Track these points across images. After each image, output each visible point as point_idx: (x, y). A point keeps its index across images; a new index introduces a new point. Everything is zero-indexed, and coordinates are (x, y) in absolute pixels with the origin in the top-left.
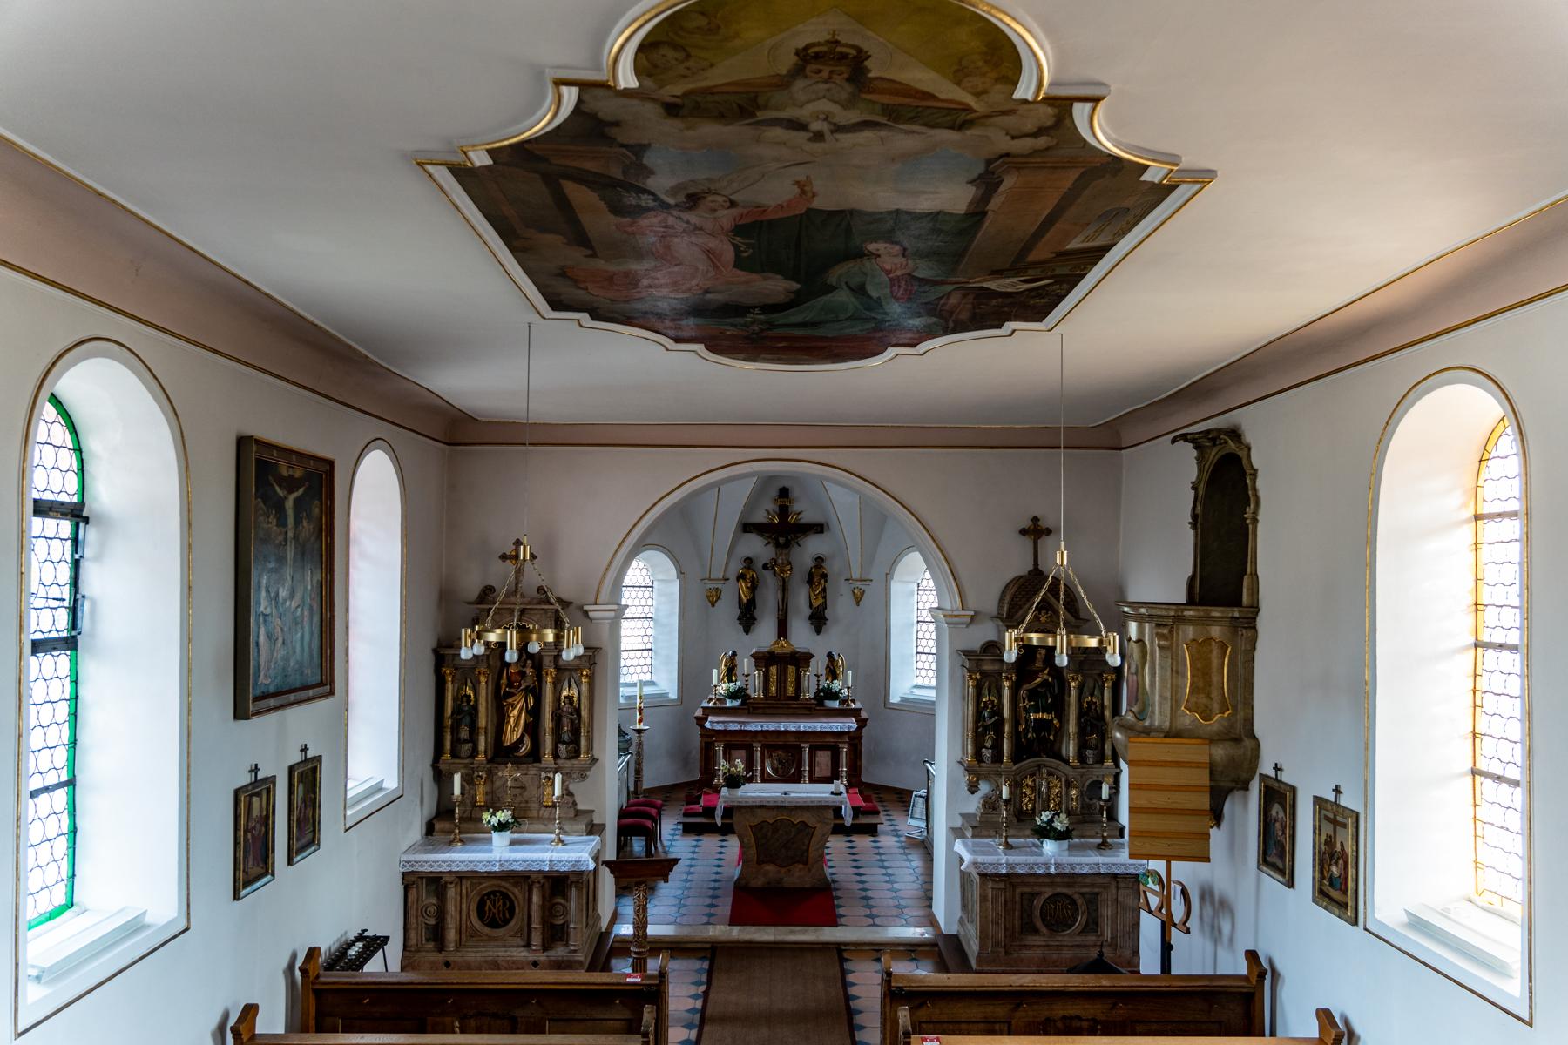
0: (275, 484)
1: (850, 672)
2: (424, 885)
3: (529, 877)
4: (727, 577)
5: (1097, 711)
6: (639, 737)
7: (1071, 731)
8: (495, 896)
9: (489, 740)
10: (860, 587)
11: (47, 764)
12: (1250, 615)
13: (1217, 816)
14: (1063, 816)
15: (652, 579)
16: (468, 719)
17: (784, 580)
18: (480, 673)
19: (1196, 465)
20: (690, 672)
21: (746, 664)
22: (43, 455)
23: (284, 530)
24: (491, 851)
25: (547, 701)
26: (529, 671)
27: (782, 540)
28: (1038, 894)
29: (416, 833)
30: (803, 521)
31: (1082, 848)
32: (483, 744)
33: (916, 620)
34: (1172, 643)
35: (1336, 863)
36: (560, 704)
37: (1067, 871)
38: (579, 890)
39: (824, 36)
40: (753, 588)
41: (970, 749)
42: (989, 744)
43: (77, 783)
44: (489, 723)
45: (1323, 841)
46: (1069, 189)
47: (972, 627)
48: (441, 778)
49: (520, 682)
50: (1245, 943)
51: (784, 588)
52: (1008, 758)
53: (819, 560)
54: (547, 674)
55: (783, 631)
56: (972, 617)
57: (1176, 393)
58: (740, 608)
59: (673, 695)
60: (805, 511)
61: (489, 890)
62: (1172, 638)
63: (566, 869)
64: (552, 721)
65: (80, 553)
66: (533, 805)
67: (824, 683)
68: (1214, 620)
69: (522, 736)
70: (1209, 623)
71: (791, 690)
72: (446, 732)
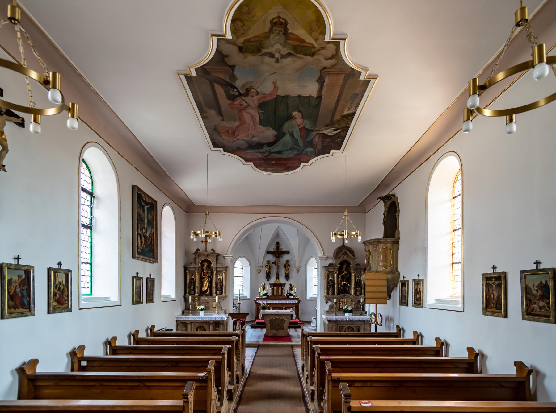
1: (296, 289)
3: (209, 322)
4: (263, 266)
6: (239, 305)
11: (85, 257)
13: (389, 297)
14: (350, 307)
16: (193, 284)
17: (278, 266)
20: (253, 291)
21: (268, 287)
22: (83, 176)
23: (144, 214)
24: (199, 315)
26: (209, 272)
27: (277, 255)
28: (344, 327)
29: (180, 312)
33: (313, 285)
34: (377, 249)
35: (418, 294)
37: (351, 320)
38: (223, 326)
39: (276, 15)
40: (270, 268)
41: (326, 292)
42: (331, 290)
43: (92, 264)
46: (342, 84)
47: (327, 261)
48: (186, 300)
51: (278, 268)
53: (288, 261)
54: (214, 272)
55: (278, 278)
57: (379, 184)
59: (248, 297)
60: (283, 248)
61: (199, 326)
63: (219, 320)
65: (92, 205)
67: (289, 292)
69: (207, 289)
71: (280, 293)
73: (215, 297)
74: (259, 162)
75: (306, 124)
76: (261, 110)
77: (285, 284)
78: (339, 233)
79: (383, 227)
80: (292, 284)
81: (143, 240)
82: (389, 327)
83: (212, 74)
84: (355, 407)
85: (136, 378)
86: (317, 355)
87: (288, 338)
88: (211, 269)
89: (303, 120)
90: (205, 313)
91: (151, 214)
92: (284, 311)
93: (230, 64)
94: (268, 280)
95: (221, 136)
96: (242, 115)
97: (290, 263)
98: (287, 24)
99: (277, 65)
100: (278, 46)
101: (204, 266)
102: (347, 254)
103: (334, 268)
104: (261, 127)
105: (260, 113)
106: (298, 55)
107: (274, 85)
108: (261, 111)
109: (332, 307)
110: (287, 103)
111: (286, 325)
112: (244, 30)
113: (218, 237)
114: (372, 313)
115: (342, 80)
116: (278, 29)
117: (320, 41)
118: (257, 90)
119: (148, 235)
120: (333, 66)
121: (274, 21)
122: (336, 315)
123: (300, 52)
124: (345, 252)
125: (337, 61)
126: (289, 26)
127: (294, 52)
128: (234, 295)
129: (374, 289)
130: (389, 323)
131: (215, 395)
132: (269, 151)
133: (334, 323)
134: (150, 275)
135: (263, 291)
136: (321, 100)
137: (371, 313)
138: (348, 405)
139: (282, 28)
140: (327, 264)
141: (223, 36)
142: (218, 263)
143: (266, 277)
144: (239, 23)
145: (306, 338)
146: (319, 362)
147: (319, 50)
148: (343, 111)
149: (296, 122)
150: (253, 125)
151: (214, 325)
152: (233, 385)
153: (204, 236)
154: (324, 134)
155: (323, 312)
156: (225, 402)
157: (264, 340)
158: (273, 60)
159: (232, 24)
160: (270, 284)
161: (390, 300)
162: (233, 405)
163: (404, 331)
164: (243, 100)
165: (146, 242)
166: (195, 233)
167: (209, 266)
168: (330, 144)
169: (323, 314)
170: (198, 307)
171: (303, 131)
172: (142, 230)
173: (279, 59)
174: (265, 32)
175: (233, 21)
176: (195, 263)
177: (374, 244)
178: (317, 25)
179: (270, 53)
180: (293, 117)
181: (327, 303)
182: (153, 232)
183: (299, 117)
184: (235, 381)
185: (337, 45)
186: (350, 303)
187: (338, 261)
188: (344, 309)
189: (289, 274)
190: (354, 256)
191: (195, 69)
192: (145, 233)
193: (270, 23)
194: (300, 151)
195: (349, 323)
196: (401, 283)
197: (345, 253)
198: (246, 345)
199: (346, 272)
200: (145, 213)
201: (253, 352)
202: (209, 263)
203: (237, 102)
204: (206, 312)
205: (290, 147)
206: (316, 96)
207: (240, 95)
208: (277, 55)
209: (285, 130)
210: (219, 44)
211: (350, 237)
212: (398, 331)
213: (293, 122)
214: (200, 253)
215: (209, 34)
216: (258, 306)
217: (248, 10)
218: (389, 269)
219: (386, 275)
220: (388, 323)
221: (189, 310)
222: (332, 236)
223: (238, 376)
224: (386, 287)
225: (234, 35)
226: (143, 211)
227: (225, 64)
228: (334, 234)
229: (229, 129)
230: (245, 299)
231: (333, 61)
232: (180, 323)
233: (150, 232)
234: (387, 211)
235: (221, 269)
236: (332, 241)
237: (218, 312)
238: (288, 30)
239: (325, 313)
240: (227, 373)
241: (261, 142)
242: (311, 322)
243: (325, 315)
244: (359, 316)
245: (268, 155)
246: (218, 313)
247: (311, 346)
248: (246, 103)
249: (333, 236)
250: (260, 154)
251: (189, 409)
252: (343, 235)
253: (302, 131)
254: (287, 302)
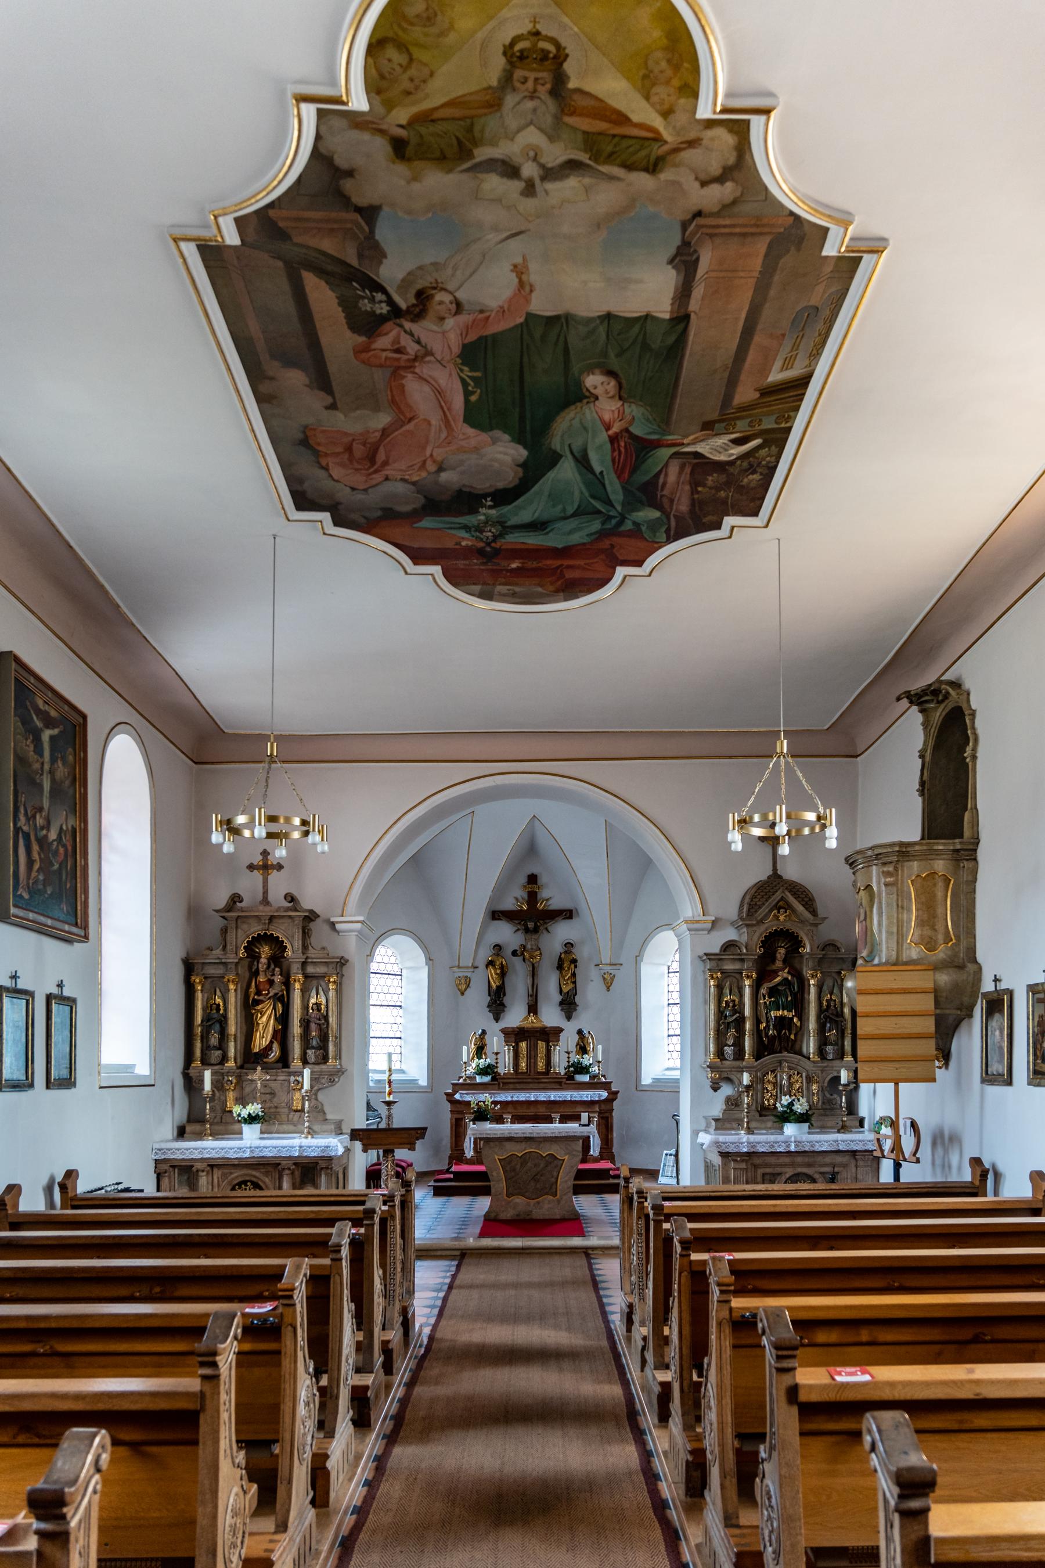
0: (32, 712)
1: (600, 1047)
2: (176, 1175)
3: (279, 1164)
4: (476, 965)
5: (836, 1008)
6: (389, 1110)
7: (811, 1027)
8: (246, 1185)
9: (239, 1048)
10: (610, 971)
12: (971, 847)
13: (945, 1056)
14: (803, 1100)
15: (400, 966)
16: (217, 1027)
17: (533, 965)
18: (229, 980)
19: (920, 729)
21: (496, 1042)
23: (41, 760)
24: (241, 1139)
25: (296, 1007)
26: (278, 979)
27: (531, 925)
28: (779, 1174)
29: (168, 1130)
30: (551, 908)
31: (823, 1129)
32: (233, 1050)
33: (666, 1003)
34: (897, 880)
36: (308, 1011)
37: (807, 1149)
39: (525, 27)
40: (503, 974)
41: (712, 1048)
42: (730, 1042)
44: (239, 1031)
45: (1036, 1024)
47: (714, 933)
48: (191, 1084)
49: (268, 991)
50: (970, 1152)
51: (534, 974)
52: (749, 1054)
53: (569, 945)
55: (533, 1008)
56: (714, 923)
57: (900, 648)
58: (489, 995)
59: (423, 1082)
60: (553, 897)
61: (240, 1179)
62: (898, 875)
63: (315, 1154)
64: (300, 1026)
66: (283, 1110)
67: (575, 1058)
68: (938, 854)
69: (271, 1042)
70: (933, 857)
71: (541, 1065)
72: (196, 1040)
73: (301, 1074)
74: (461, 563)
75: (633, 418)
76: (471, 370)
77: (560, 1030)
78: (757, 818)
79: (919, 801)
80: (585, 1032)
81: (35, 856)
82: (946, 1166)
83: (295, 240)
84: (811, 1387)
85: (22, 1325)
86: (679, 1249)
87: (574, 1224)
88: (285, 967)
89: (623, 405)
90: (262, 1133)
91: (63, 759)
92: (556, 1128)
93: (361, 200)
94: (497, 1019)
95: (326, 469)
96: (402, 387)
97: (578, 953)
98: (565, 60)
99: (529, 205)
100: (532, 137)
101: (260, 957)
102: (788, 906)
103: (742, 960)
104: (470, 431)
105: (468, 380)
106: (604, 169)
107: (517, 276)
108: (469, 374)
109: (737, 1105)
110: (566, 342)
111: (565, 1179)
112: (412, 80)
113: (314, 838)
114: (881, 1118)
115: (759, 260)
116: (532, 76)
117: (680, 118)
118: (458, 295)
119: (53, 835)
120: (728, 207)
121: (518, 47)
122: (750, 1131)
123: (609, 158)
124: (782, 899)
125: (740, 189)
126: (569, 67)
127: (590, 159)
128: (370, 1075)
129: (887, 1026)
130: (946, 1152)
131: (308, 1387)
132: (501, 523)
133: (743, 1161)
134: (60, 985)
135: (480, 1058)
136: (685, 330)
137: (877, 1118)
138: (787, 1380)
139: (543, 71)
140: (715, 943)
141: (338, 101)
142: (310, 948)
143: (489, 1006)
144: (391, 52)
145: (638, 1202)
146: (685, 1274)
147: (676, 150)
148: (765, 370)
149: (597, 413)
150: (443, 427)
151: (297, 1173)
152: (372, 1372)
153: (260, 832)
154: (697, 455)
155: (703, 1125)
156: (344, 1427)
157: (483, 1234)
158: (515, 186)
159: (370, 60)
160: (502, 1031)
161: (947, 1068)
162: (372, 1443)
163: (997, 1176)
164: (405, 331)
165: (46, 863)
166: (229, 822)
167: (278, 959)
168: (722, 494)
169: (701, 1131)
170: (237, 1109)
171: (622, 444)
172: (31, 819)
173: (537, 181)
174: (485, 85)
175: (375, 47)
176: (225, 947)
177: (884, 864)
178: (669, 61)
179: (504, 162)
180: (587, 394)
181: (715, 1090)
182: (72, 826)
183: (607, 392)
184: (379, 1360)
185: (741, 131)
186: (801, 1087)
187: (757, 934)
188: (780, 1109)
189: (576, 994)
190: (814, 913)
191: (237, 220)
192: (42, 828)
193: (505, 53)
194: (614, 522)
195: (799, 1159)
196: (987, 1002)
197: (781, 903)
198: (417, 1250)
199: (785, 974)
200: (41, 755)
201: (442, 1274)
202: (278, 946)
203: (383, 342)
204: (264, 1127)
205: (576, 507)
206: (667, 316)
207: (396, 312)
208: (529, 170)
209: (556, 444)
210: (323, 129)
211: (799, 831)
212: (978, 1178)
213: (588, 413)
214: (242, 910)
215: (289, 95)
216: (462, 1113)
217: (427, 9)
218: (941, 952)
219: (931, 973)
220: (940, 1151)
221: (202, 1121)
222: (731, 828)
223: (390, 1346)
224: (933, 1018)
225: (377, 100)
226: (35, 747)
227: (345, 201)
228: (739, 822)
229: (354, 440)
230: (410, 1087)
231: (727, 191)
232: (171, 1169)
233: (61, 828)
234: (931, 743)
235: (321, 970)
236: (733, 847)
237: (309, 1127)
238: (568, 78)
239: (708, 1126)
240: (349, 1336)
241: (471, 487)
242: (658, 1171)
243: (706, 1131)
244: (834, 1133)
245: (495, 538)
246: (311, 1132)
247: (659, 1224)
248: (418, 342)
249: (734, 829)
250: (467, 535)
251: (222, 1408)
252: (773, 825)
253: (619, 446)
254: (568, 1095)
